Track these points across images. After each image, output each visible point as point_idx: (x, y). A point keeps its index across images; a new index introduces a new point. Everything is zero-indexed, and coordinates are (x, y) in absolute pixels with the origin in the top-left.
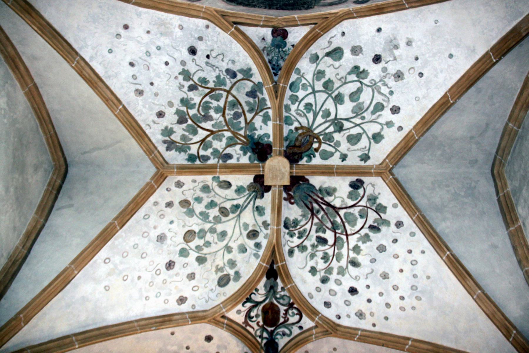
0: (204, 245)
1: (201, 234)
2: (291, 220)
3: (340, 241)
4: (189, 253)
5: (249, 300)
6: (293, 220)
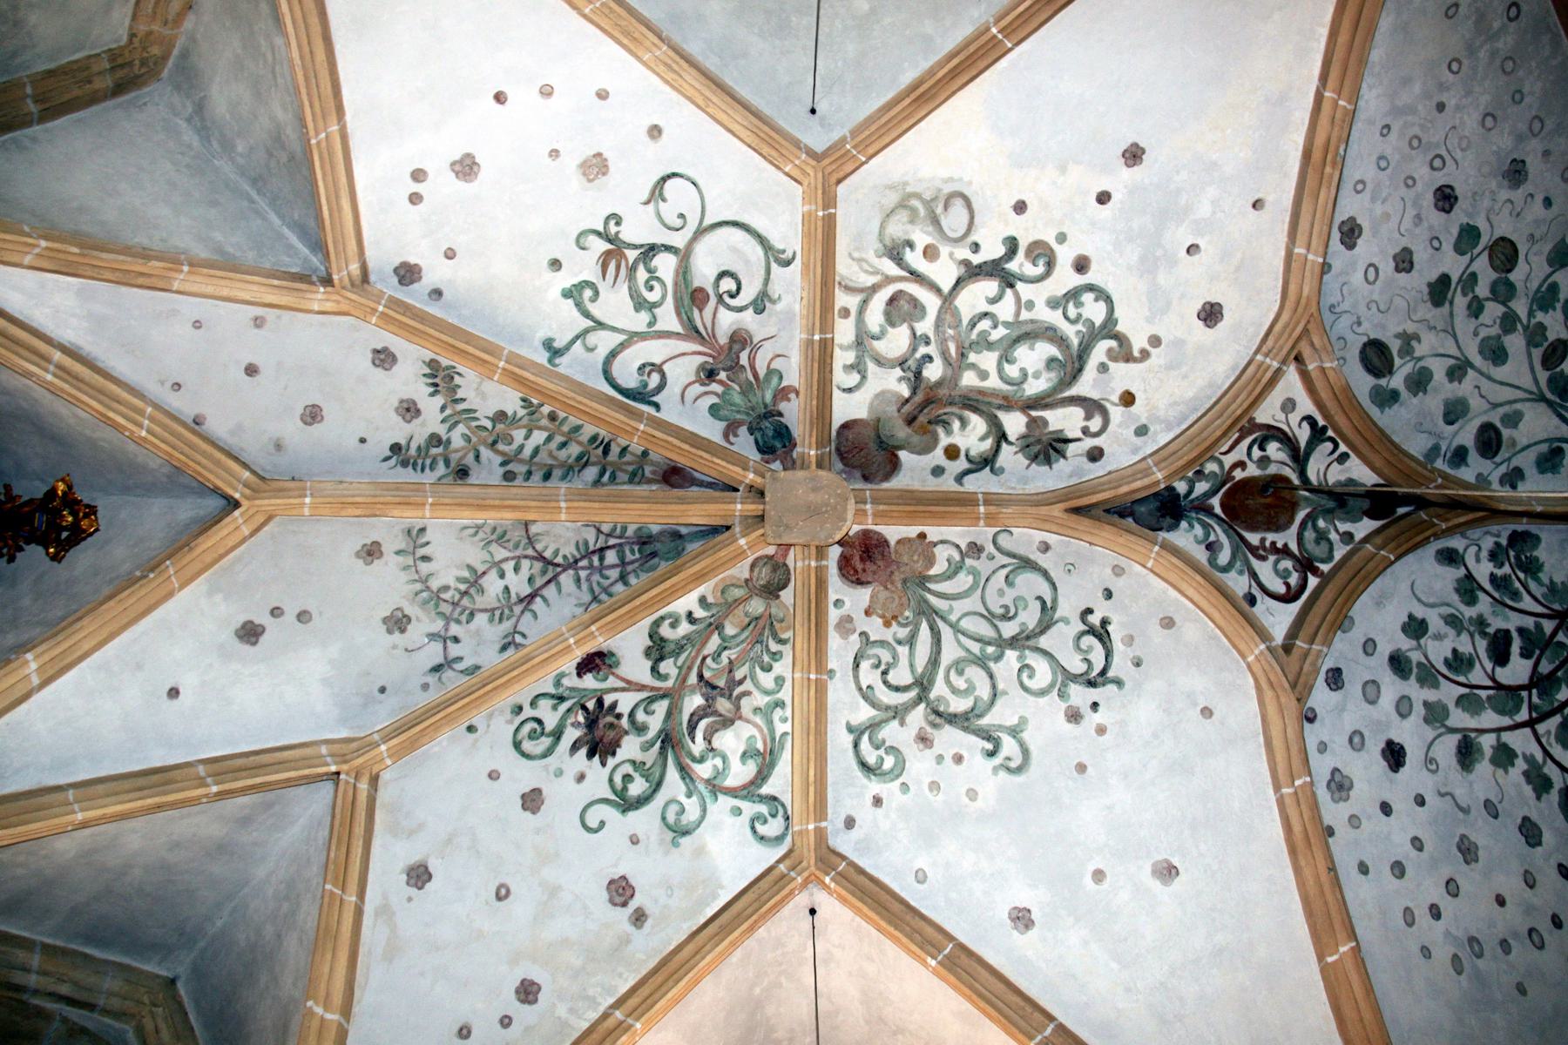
0: (1475, 297)
1: (1502, 289)
2: (1535, 553)
3: (1511, 704)
4: (1462, 254)
5: (1318, 434)
6: (1537, 559)
